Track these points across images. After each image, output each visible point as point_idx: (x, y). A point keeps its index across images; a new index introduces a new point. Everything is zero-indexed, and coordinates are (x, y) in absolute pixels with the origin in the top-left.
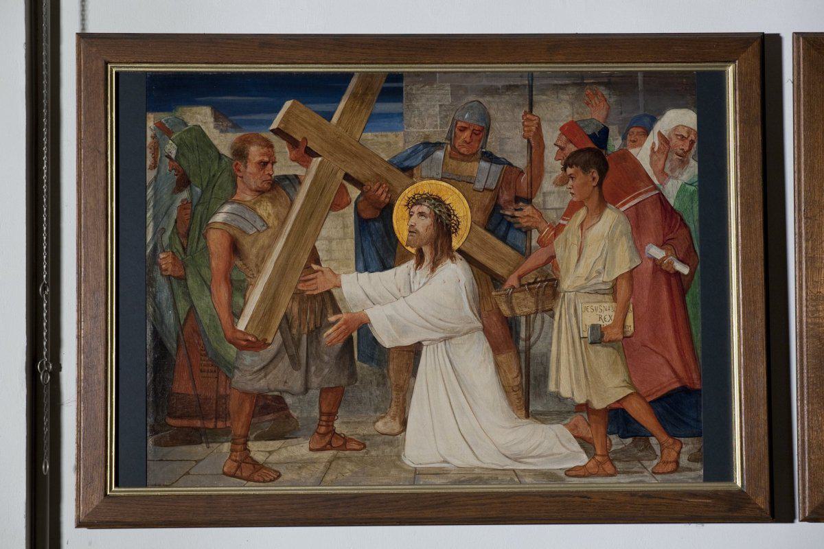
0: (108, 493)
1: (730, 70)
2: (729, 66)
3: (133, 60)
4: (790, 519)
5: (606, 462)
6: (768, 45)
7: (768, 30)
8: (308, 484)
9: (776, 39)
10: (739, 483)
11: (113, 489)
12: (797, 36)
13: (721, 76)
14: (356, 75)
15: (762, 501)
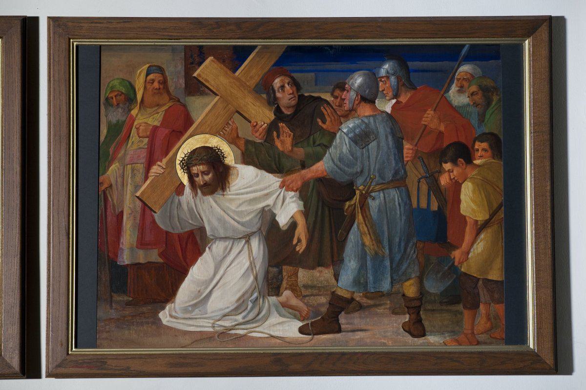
0: (70, 352)
3: (237, 37)
4: (38, 376)
5: (417, 329)
6: (29, 25)
7: (554, 14)
8: (250, 346)
9: (35, 20)
11: (74, 349)
13: (519, 49)
14: (259, 47)
15: (549, 360)
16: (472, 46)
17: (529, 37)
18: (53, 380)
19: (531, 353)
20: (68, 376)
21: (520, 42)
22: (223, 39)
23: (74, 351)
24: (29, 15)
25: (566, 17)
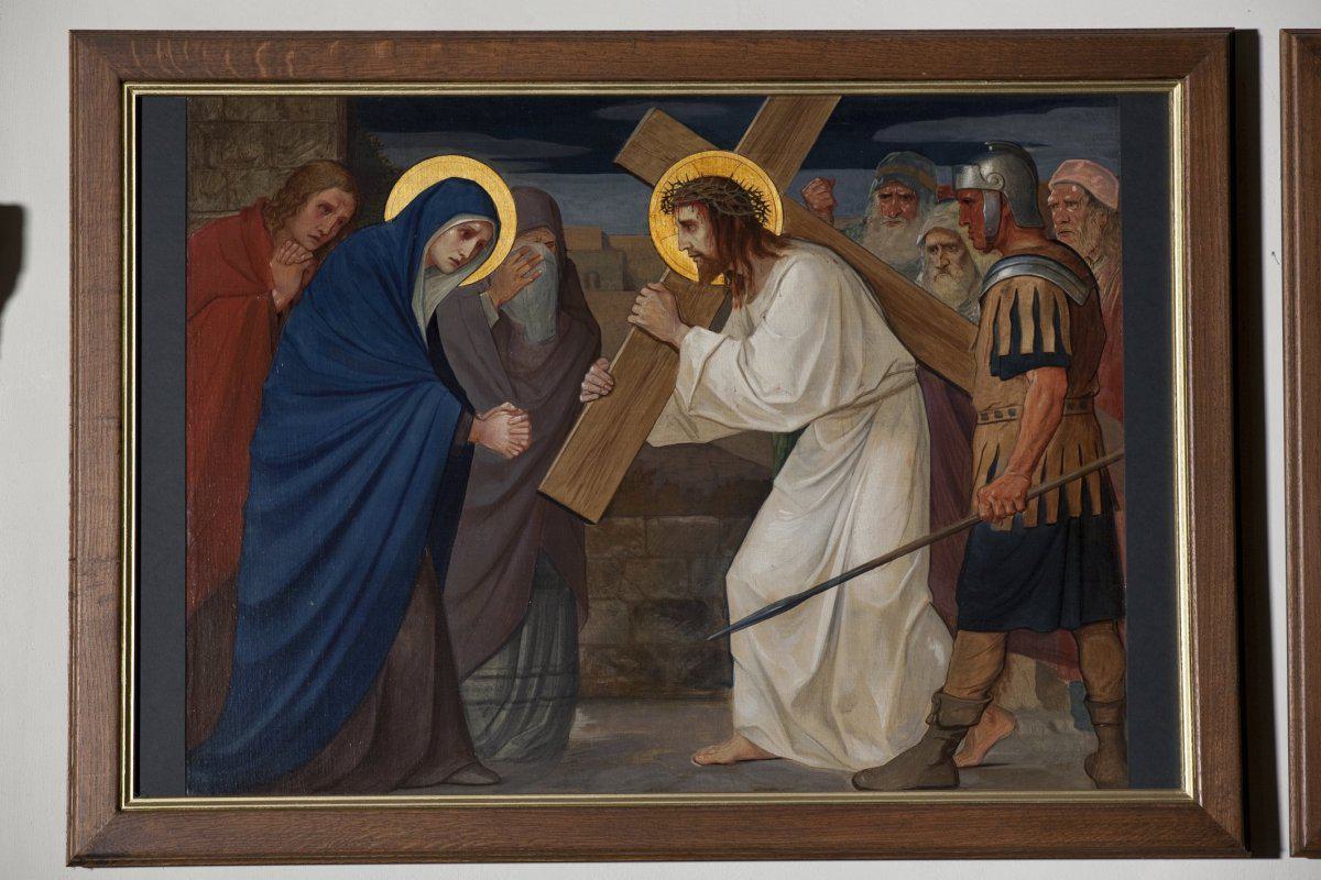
0: (124, 807)
1: (1177, 91)
2: (1175, 85)
4: (1272, 851)
6: (1241, 46)
10: (1189, 789)
11: (132, 799)
12: (1288, 34)
13: (1163, 100)
15: (1229, 818)
16: (846, 100)
17: (1181, 78)
18: (79, 869)
19: (1191, 808)
20: (426, 858)
21: (1166, 89)
22: (988, 81)
24: (1238, 26)
25: (1262, 33)
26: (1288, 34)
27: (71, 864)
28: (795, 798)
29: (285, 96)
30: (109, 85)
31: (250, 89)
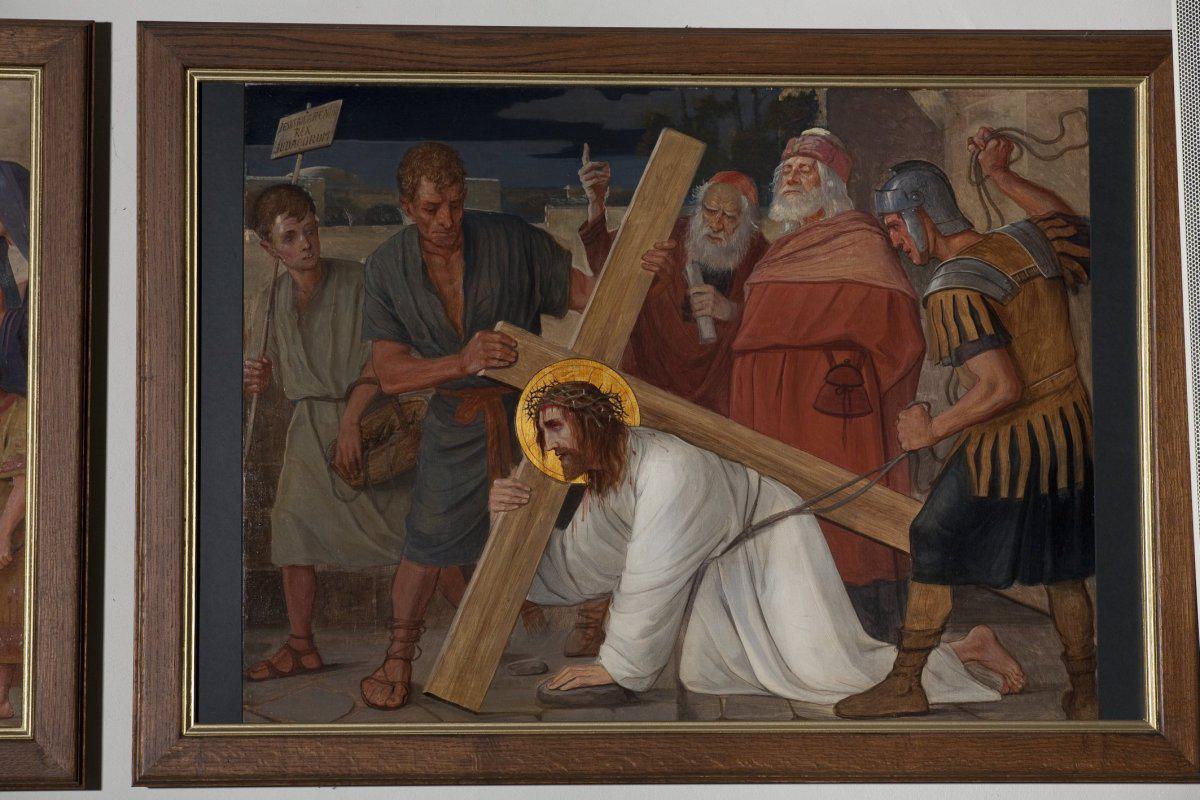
1: (1142, 90)
6: (96, 37)
9: (105, 29)
10: (1152, 721)
12: (144, 27)
13: (1129, 96)
18: (143, 790)
19: (1153, 734)
21: (1132, 85)
23: (194, 730)
26: (144, 27)
27: (136, 783)
28: (764, 727)
29: (740, 87)
30: (177, 68)
31: (576, 79)
